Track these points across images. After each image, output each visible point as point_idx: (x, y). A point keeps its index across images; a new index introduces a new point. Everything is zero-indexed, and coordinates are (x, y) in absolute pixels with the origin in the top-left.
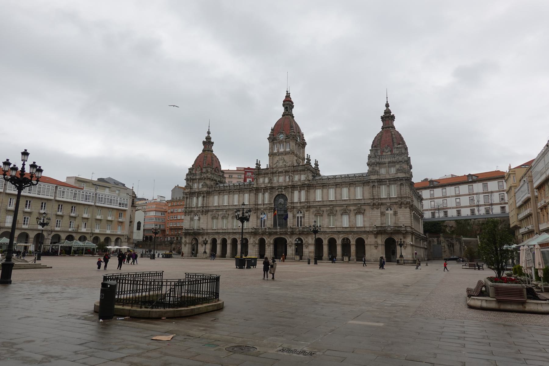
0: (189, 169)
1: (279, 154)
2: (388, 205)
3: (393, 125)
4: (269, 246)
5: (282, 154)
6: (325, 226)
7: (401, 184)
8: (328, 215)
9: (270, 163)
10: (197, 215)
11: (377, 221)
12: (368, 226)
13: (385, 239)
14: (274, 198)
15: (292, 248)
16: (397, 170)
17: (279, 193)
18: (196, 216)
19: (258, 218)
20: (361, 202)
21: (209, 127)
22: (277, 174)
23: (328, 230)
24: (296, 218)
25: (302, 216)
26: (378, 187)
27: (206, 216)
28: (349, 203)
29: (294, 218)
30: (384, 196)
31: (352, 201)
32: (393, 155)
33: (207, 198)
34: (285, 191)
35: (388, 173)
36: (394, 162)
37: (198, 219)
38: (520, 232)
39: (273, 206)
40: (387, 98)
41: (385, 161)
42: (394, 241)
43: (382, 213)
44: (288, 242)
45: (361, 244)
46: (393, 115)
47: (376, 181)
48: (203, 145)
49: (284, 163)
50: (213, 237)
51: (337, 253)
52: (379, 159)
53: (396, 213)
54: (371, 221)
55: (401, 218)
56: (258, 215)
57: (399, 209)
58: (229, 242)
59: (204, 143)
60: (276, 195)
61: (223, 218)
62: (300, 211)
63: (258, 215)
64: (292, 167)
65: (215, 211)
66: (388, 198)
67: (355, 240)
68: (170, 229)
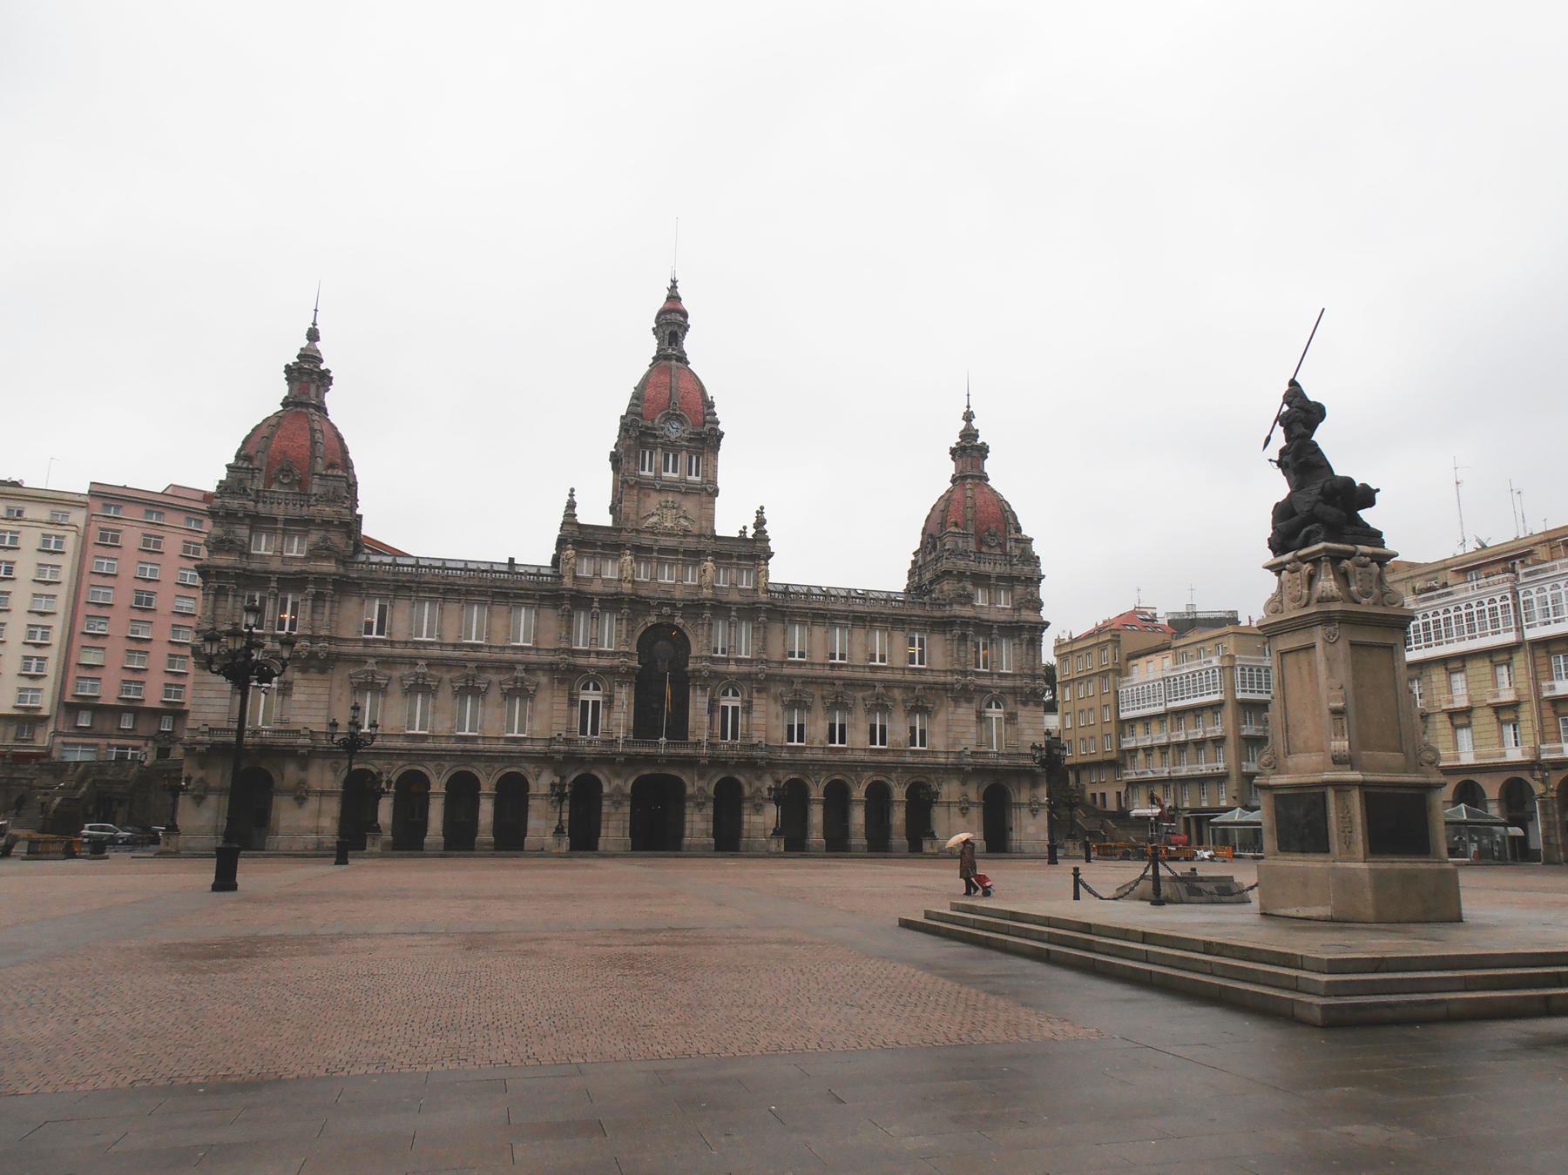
3: (982, 471)
12: (942, 749)
15: (704, 812)
16: (312, 548)
17: (660, 621)
19: (572, 702)
25: (736, 704)
29: (981, 722)
30: (474, 637)
31: (818, 667)
32: (305, 498)
34: (681, 617)
39: (635, 664)
40: (968, 395)
41: (275, 511)
42: (739, 787)
46: (984, 443)
52: (256, 502)
57: (1020, 706)
66: (268, 635)
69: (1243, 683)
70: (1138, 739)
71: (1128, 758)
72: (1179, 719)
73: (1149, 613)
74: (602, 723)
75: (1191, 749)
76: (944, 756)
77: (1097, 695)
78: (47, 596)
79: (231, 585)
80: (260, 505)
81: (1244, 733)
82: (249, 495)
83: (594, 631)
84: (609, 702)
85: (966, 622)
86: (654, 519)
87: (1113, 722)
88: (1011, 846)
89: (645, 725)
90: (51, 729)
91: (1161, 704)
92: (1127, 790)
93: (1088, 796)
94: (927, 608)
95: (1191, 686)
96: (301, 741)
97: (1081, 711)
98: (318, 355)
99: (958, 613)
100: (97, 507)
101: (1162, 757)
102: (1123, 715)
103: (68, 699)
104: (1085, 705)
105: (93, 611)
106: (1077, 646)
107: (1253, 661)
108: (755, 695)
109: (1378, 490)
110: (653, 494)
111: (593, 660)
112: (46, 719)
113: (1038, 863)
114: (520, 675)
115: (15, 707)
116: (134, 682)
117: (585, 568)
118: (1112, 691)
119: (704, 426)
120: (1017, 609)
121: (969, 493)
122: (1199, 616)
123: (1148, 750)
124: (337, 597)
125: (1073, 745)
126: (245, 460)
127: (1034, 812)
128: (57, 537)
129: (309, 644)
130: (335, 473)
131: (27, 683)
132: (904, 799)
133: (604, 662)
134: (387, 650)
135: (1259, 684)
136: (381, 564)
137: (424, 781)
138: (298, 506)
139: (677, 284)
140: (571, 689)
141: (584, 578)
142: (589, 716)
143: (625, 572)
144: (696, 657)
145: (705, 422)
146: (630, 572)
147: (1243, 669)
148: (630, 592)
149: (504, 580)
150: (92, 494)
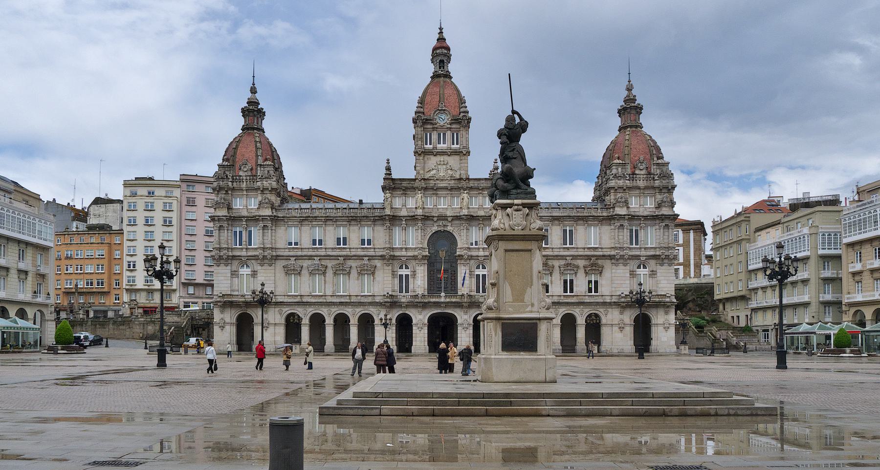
2: (642, 259)
5: (445, 152)
7: (264, 226)
11: (624, 286)
13: (237, 315)
17: (439, 229)
18: (243, 266)
21: (254, 77)
22: (245, 193)
23: (286, 300)
26: (272, 230)
27: (272, 267)
28: (349, 253)
29: (471, 278)
36: (256, 189)
39: (427, 253)
43: (632, 273)
44: (414, 322)
46: (639, 104)
51: (578, 340)
53: (255, 273)
54: (614, 285)
55: (662, 282)
57: (659, 267)
59: (245, 112)
61: (311, 274)
62: (247, 265)
66: (244, 248)
67: (333, 317)
68: (64, 292)
71: (753, 294)
73: (776, 200)
74: (411, 287)
76: (609, 298)
77: (735, 256)
78: (169, 232)
79: (225, 224)
80: (235, 184)
82: (229, 179)
83: (404, 237)
84: (414, 273)
86: (434, 172)
88: (651, 349)
89: (433, 285)
90: (178, 295)
94: (599, 210)
95: (798, 246)
97: (726, 266)
98: (256, 101)
99: (618, 213)
100: (184, 185)
102: (751, 268)
103: (183, 281)
104: (728, 262)
105: (189, 238)
106: (724, 225)
107: (831, 228)
109: (535, 169)
110: (432, 157)
111: (404, 253)
112: (174, 290)
113: (634, 358)
114: (365, 263)
116: (210, 271)
117: (398, 202)
118: (744, 253)
119: (460, 115)
120: (659, 206)
121: (627, 138)
122: (811, 199)
125: (721, 286)
126: (227, 161)
127: (666, 329)
128: (169, 203)
129: (262, 252)
130: (267, 164)
132: (585, 323)
133: (410, 254)
134: (300, 253)
135: (830, 244)
138: (252, 182)
139: (443, 31)
142: (404, 282)
143: (418, 203)
144: (461, 248)
145: (460, 113)
146: (421, 203)
148: (421, 214)
150: (182, 181)
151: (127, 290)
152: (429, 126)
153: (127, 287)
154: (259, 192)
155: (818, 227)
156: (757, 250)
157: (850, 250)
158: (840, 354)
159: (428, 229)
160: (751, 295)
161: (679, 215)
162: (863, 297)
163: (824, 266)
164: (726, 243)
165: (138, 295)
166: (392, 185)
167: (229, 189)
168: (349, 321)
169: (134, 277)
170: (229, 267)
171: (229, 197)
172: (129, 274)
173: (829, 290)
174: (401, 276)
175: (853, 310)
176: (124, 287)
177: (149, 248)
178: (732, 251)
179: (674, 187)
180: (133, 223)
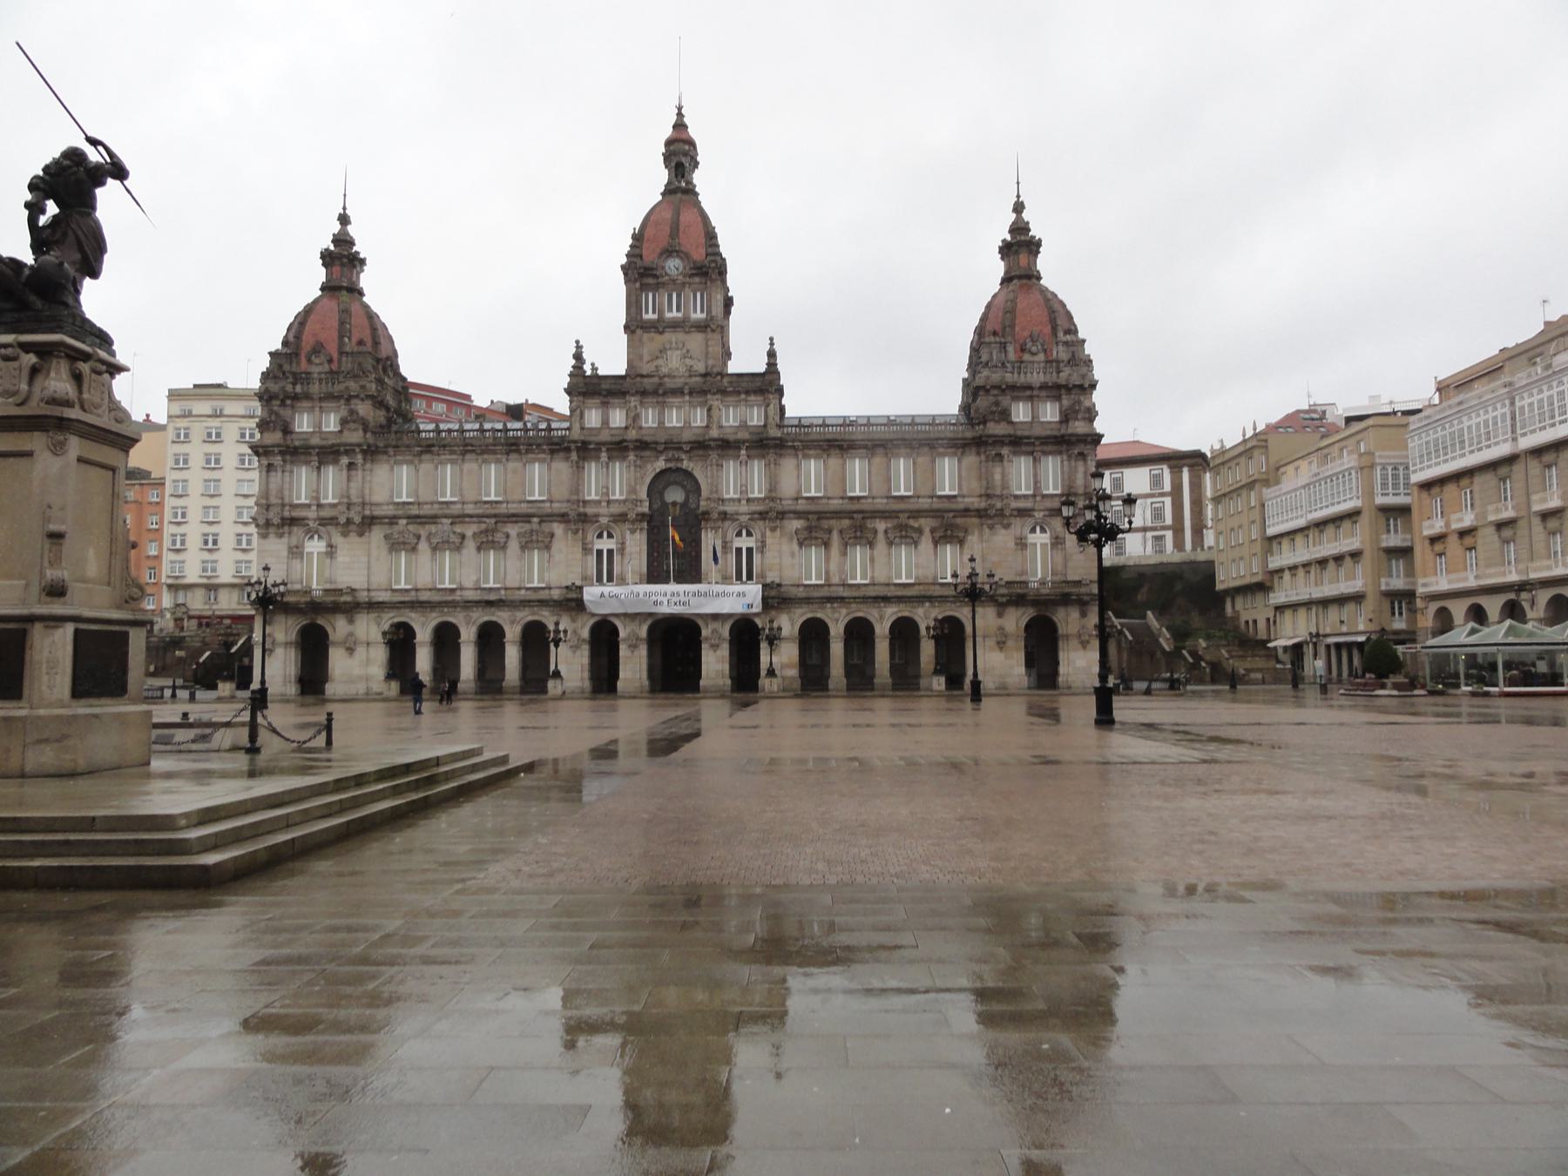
0: (270, 354)
1: (658, 327)
4: (633, 647)
6: (470, 585)
8: (936, 543)
9: (631, 356)
10: (320, 537)
13: (298, 627)
14: (648, 480)
15: (718, 652)
18: (312, 537)
19: (586, 550)
20: (953, 506)
21: (1018, 183)
24: (592, 554)
25: (750, 545)
30: (947, 488)
33: (283, 471)
35: (605, 422)
37: (324, 550)
38: (1271, 602)
45: (951, 637)
47: (276, 450)
48: (1002, 259)
49: (688, 361)
50: (396, 620)
52: (1012, 373)
56: (587, 541)
58: (468, 635)
59: (327, 258)
60: (658, 470)
63: (587, 541)
64: (719, 377)
65: (404, 522)
69: (1385, 485)
70: (1284, 557)
71: (1276, 580)
72: (1321, 531)
75: (1331, 565)
78: (249, 481)
79: (278, 460)
81: (1384, 544)
85: (999, 441)
87: (1259, 540)
91: (1302, 516)
92: (1275, 616)
93: (1243, 625)
96: (343, 599)
97: (1232, 530)
101: (1305, 576)
102: (1271, 531)
106: (1227, 456)
107: (1394, 457)
108: (768, 533)
115: (201, 577)
120: (1066, 418)
123: (1293, 568)
124: (368, 466)
131: (241, 556)
135: (1396, 486)
136: (450, 431)
137: (502, 633)
140: (584, 538)
141: (1022, 423)
147: (1384, 469)
149: (925, 432)
151: (170, 586)
152: (651, 281)
153: (170, 581)
154: (342, 402)
155: (1374, 454)
156: (1279, 500)
157: (1425, 495)
158: (1373, 690)
159: (649, 466)
160: (1272, 581)
161: (1103, 436)
162: (1450, 582)
163: (1388, 525)
164: (1232, 488)
165: (189, 594)
166: (585, 386)
167: (287, 397)
168: (504, 637)
169: (216, 561)
170: (285, 540)
171: (286, 413)
172: (172, 556)
173: (1398, 571)
174: (600, 552)
175: (1434, 607)
176: (163, 581)
177: (211, 510)
178: (1239, 504)
179: (1093, 386)
180: (182, 463)
